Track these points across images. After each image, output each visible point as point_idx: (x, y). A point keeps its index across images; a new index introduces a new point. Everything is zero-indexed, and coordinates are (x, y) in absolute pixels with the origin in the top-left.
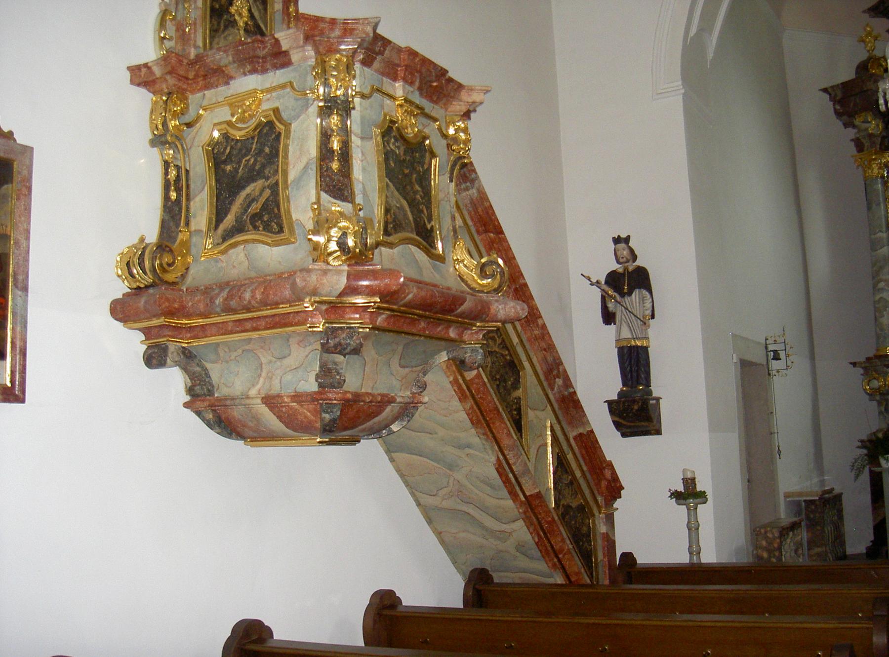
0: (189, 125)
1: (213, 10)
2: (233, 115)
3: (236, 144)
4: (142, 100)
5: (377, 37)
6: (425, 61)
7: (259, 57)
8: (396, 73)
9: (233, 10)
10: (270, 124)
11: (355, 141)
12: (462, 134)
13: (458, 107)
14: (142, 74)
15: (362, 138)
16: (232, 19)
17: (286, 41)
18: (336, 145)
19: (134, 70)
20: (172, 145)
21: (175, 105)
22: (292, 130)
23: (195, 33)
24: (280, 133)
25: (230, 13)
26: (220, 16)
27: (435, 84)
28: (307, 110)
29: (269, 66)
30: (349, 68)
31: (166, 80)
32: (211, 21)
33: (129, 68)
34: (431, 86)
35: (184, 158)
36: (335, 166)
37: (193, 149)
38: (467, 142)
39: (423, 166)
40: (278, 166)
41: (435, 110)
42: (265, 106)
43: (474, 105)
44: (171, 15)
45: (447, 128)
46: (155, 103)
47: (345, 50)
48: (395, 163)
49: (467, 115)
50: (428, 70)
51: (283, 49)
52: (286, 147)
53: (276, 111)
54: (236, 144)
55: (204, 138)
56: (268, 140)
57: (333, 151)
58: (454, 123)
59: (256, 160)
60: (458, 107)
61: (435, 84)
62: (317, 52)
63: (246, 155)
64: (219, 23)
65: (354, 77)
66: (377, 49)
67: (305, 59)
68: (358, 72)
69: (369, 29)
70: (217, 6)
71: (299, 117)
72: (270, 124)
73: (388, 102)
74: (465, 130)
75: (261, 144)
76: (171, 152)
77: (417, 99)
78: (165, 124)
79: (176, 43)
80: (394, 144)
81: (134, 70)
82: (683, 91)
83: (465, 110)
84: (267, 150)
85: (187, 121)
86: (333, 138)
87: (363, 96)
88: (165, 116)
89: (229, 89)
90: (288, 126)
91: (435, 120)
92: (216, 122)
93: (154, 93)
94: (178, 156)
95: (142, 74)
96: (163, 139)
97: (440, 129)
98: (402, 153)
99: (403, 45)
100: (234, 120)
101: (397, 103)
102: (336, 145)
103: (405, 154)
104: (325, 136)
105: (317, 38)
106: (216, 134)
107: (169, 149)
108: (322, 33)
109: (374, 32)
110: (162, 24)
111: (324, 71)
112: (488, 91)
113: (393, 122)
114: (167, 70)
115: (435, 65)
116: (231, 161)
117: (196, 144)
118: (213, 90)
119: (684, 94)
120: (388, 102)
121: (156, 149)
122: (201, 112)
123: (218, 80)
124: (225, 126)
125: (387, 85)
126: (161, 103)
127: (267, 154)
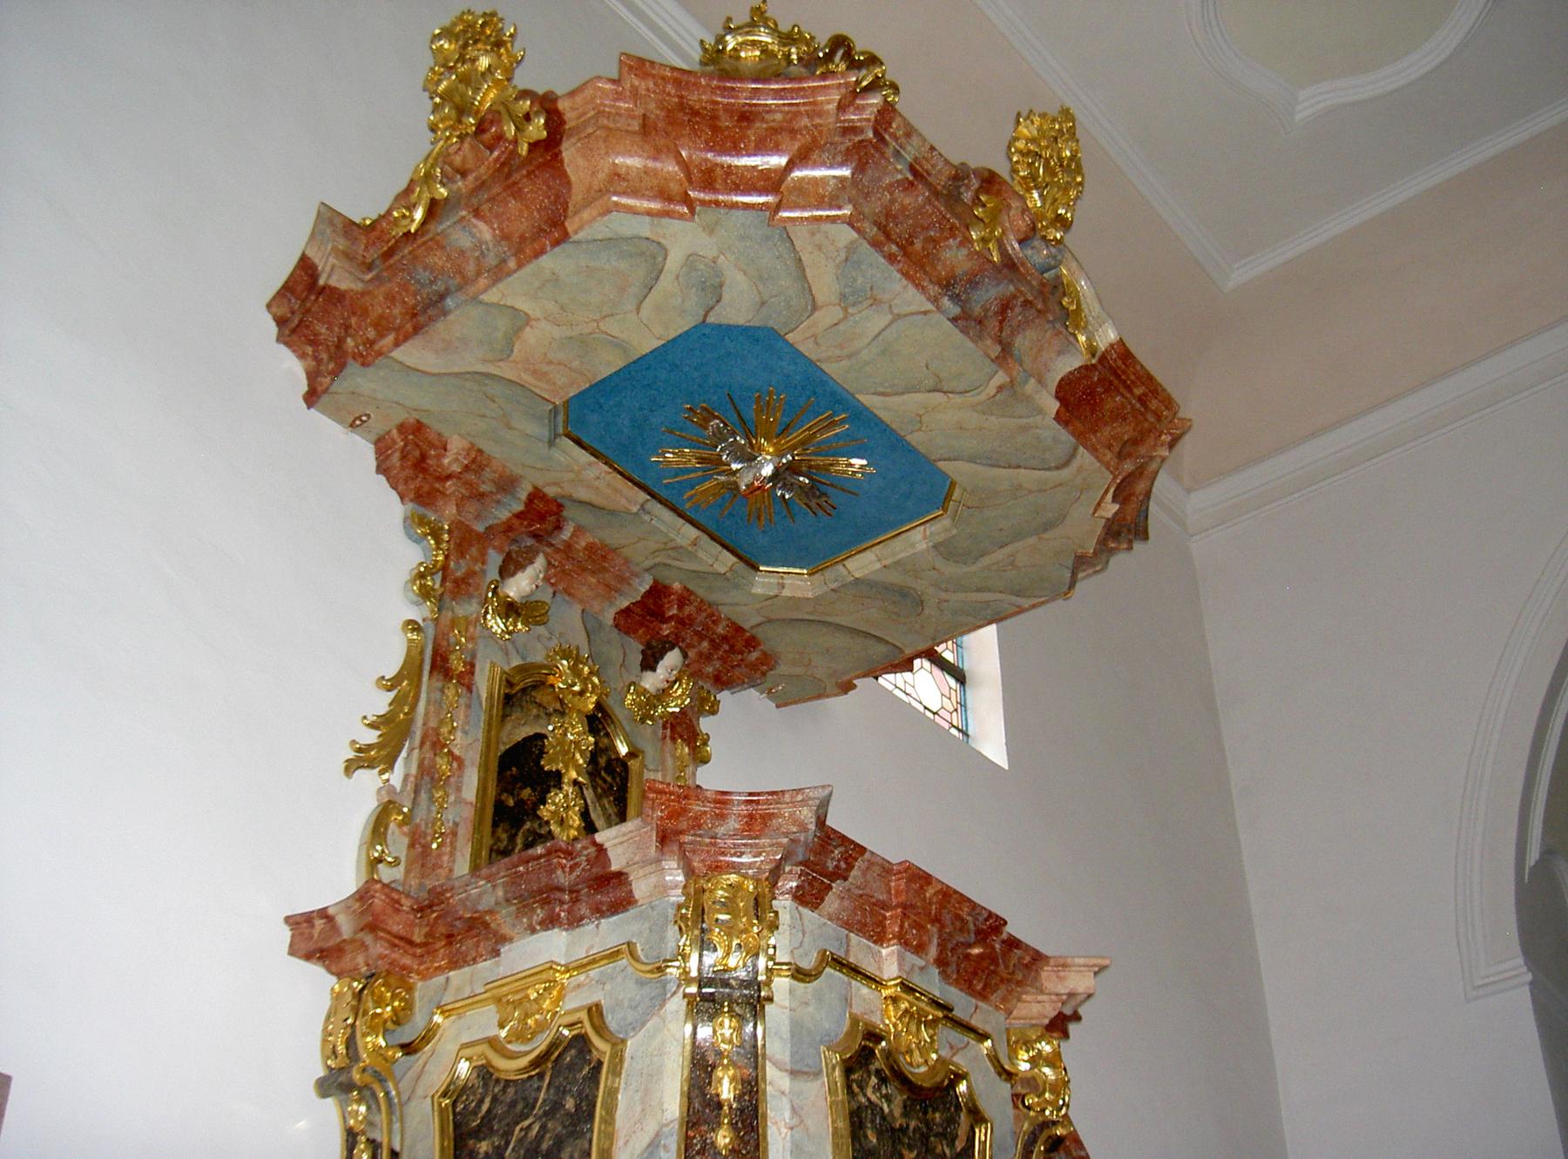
0: (409, 1049)
1: (499, 806)
2: (502, 1026)
3: (504, 1090)
4: (314, 990)
5: (828, 838)
6: (948, 895)
7: (560, 889)
8: (881, 923)
9: (545, 812)
10: (581, 1041)
11: (776, 1080)
12: (1046, 1070)
13: (1035, 1009)
14: (316, 932)
15: (794, 1073)
16: (543, 831)
17: (620, 850)
18: (726, 1090)
19: (300, 924)
20: (366, 1093)
21: (379, 1002)
22: (627, 1055)
23: (452, 854)
24: (600, 1063)
25: (539, 818)
26: (516, 824)
27: (976, 951)
28: (662, 1006)
29: (584, 909)
30: (760, 907)
31: (364, 946)
32: (494, 833)
33: (288, 920)
34: (968, 957)
35: (390, 1123)
36: (723, 1138)
37: (413, 1103)
38: (1060, 1087)
39: (952, 1144)
40: (590, 1141)
41: (982, 1015)
42: (571, 1003)
43: (1073, 1003)
44: (400, 812)
45: (1013, 1056)
46: (337, 997)
47: (750, 866)
48: (879, 1134)
49: (1059, 1025)
50: (958, 917)
51: (614, 867)
52: (612, 1093)
53: (595, 1011)
54: (504, 1090)
55: (436, 1079)
56: (575, 1080)
57: (720, 1105)
58: (1028, 1044)
59: (543, 1127)
60: (1036, 1007)
61: (979, 953)
62: (690, 872)
63: (524, 1117)
64: (512, 838)
65: (773, 927)
66: (831, 865)
67: (664, 889)
68: (785, 918)
69: (807, 815)
70: (511, 803)
71: (643, 1024)
72: (581, 1041)
73: (864, 990)
74: (1054, 1061)
75: (557, 1088)
76: (363, 1109)
77: (933, 983)
78: (351, 1043)
79: (407, 872)
80: (877, 1089)
81: (300, 924)
82: (1529, 977)
83: (1053, 1014)
84: (570, 1104)
85: (406, 1040)
86: (719, 1073)
87: (799, 974)
88: (353, 1026)
89: (497, 964)
90: (618, 1045)
91: (983, 1037)
92: (465, 1039)
93: (339, 975)
94: (377, 1119)
95: (316, 932)
96: (342, 1079)
97: (994, 1058)
98: (897, 1112)
99: (894, 858)
100: (503, 1033)
101: (885, 993)
102: (726, 1090)
103: (905, 1114)
104: (702, 1066)
105: (687, 838)
106: (464, 1068)
107: (359, 1101)
108: (697, 823)
109: (821, 822)
110: (378, 829)
111: (700, 913)
112: (1102, 968)
113: (874, 1036)
114: (364, 922)
115: (974, 906)
116: (491, 1129)
117: (420, 1092)
118: (467, 969)
119: (1531, 983)
120: (865, 991)
121: (330, 1100)
122: (438, 1019)
123: (477, 945)
124: (484, 1048)
125: (859, 950)
126: (349, 997)
127: (568, 1114)
